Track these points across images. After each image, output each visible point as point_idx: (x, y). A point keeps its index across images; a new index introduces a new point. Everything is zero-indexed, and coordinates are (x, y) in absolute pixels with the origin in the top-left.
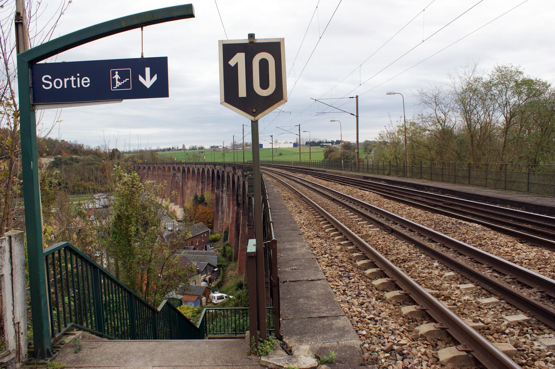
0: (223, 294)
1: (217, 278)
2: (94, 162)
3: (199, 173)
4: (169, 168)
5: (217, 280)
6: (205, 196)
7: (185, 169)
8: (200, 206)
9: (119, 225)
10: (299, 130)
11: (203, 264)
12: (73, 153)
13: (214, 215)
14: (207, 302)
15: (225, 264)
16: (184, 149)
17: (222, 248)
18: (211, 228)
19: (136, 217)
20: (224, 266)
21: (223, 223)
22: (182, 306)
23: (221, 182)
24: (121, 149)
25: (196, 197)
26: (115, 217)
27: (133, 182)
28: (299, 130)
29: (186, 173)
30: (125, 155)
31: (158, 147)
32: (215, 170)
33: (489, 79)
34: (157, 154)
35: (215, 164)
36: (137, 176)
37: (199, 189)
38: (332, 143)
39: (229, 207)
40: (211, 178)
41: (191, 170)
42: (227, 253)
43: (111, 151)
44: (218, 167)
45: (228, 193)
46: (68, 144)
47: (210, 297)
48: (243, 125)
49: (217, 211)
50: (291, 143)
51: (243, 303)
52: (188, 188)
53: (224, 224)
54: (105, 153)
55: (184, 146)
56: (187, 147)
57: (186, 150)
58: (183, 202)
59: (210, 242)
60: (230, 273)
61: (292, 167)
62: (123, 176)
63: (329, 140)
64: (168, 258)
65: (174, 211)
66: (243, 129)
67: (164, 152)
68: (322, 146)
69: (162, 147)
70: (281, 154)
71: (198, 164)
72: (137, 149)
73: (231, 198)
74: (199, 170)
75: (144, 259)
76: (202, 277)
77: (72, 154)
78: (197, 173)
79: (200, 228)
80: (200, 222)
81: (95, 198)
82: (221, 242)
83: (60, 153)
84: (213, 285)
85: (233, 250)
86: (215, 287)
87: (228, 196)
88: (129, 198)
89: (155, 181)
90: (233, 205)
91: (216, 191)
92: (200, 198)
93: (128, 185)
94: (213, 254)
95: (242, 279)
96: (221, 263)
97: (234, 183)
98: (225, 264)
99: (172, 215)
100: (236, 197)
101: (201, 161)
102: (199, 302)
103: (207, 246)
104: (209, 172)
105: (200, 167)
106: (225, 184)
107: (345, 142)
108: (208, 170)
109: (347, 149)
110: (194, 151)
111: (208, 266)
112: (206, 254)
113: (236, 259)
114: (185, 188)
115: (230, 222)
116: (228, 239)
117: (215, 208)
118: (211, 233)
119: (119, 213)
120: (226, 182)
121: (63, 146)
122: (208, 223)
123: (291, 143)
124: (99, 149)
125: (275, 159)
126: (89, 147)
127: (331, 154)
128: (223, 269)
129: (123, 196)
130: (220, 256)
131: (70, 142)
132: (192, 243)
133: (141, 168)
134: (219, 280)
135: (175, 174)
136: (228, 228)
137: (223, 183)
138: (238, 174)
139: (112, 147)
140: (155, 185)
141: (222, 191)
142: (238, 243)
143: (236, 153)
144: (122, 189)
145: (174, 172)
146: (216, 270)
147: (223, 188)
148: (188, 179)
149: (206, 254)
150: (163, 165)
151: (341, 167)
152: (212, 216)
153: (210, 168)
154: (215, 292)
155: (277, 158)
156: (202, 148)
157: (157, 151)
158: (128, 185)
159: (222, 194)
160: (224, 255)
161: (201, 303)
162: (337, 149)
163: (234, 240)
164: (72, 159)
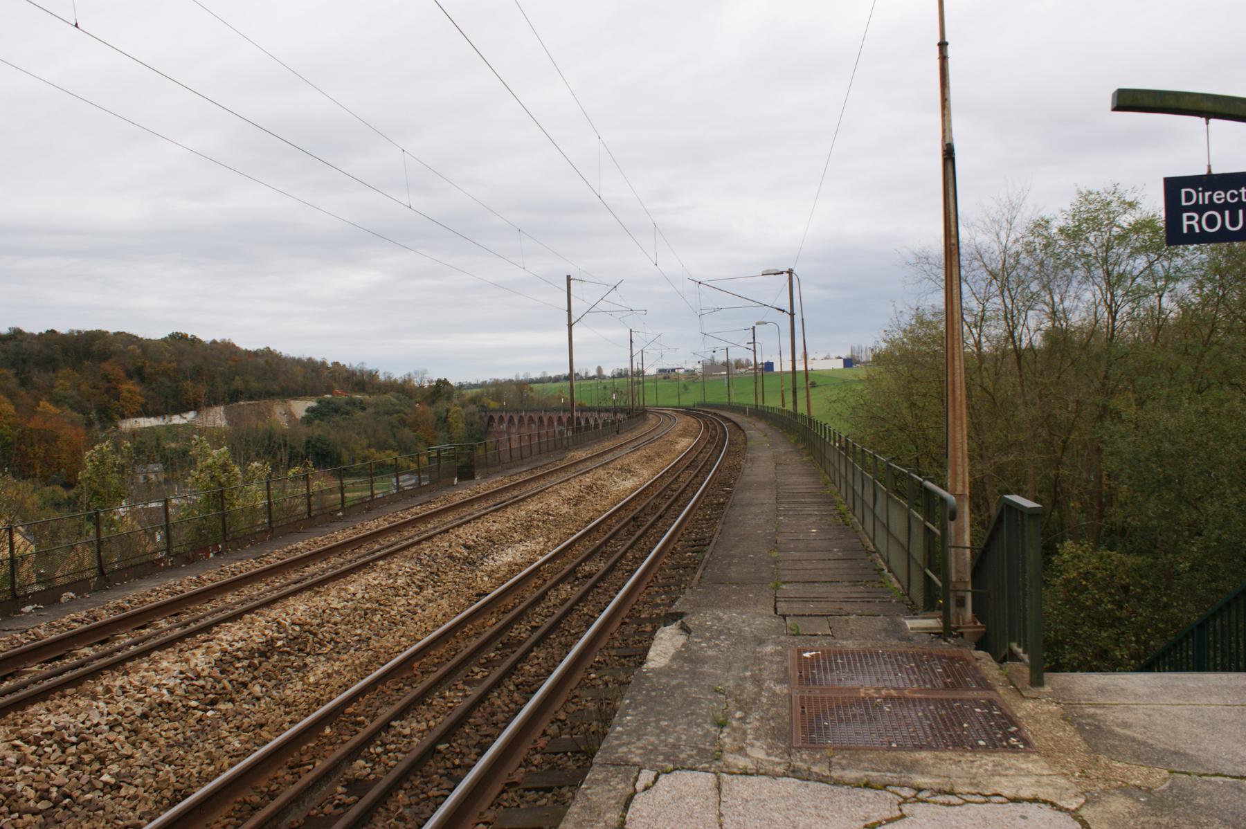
2: (397, 407)
4: (550, 419)
12: (357, 389)
16: (600, 376)
24: (453, 381)
30: (464, 392)
31: (544, 373)
34: (531, 389)
46: (347, 371)
50: (840, 358)
54: (421, 387)
55: (599, 370)
56: (607, 372)
57: (604, 378)
77: (355, 391)
83: (330, 390)
121: (337, 374)
123: (840, 358)
124: (410, 380)
126: (389, 377)
131: (351, 366)
139: (435, 375)
145: (560, 427)
164: (353, 403)
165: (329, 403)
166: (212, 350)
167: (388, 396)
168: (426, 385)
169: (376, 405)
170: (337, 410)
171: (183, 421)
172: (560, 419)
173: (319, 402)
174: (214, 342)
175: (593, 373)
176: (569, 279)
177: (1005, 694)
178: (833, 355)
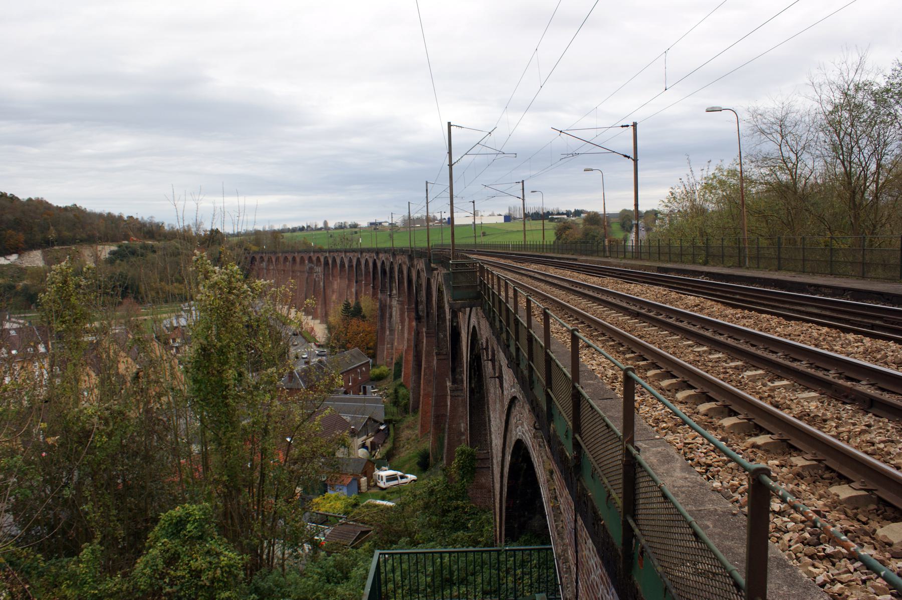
1: (384, 442)
3: (351, 266)
5: (385, 445)
6: (363, 305)
7: (328, 261)
8: (354, 321)
9: (205, 366)
10: (523, 189)
13: (377, 335)
14: (369, 485)
17: (391, 391)
18: (373, 356)
19: (238, 349)
20: (395, 421)
22: (327, 495)
23: (387, 280)
25: (347, 306)
26: (197, 350)
27: (230, 282)
28: (523, 189)
29: (331, 266)
30: (230, 239)
31: (285, 225)
32: (377, 261)
33: (883, 84)
34: (283, 236)
35: (378, 251)
36: (239, 272)
37: (351, 292)
38: (568, 214)
39: (402, 321)
40: (371, 274)
41: (338, 262)
43: (208, 233)
44: (382, 256)
45: (400, 299)
46: (139, 223)
49: (383, 329)
50: (500, 215)
52: (333, 292)
53: (394, 351)
55: (326, 223)
56: (331, 225)
58: (326, 315)
60: (406, 434)
61: (511, 254)
62: (212, 271)
63: (563, 209)
64: (299, 426)
65: (312, 329)
67: (295, 234)
68: (552, 220)
69: (290, 226)
70: (484, 234)
71: (349, 252)
72: (250, 228)
74: (350, 261)
75: (254, 431)
76: (359, 441)
78: (349, 266)
79: (354, 358)
81: (182, 309)
82: (389, 380)
83: (127, 237)
85: (411, 394)
86: (382, 459)
87: (401, 303)
88: (222, 315)
89: (273, 281)
90: (410, 319)
91: (379, 296)
92: (355, 308)
93: (220, 289)
94: (376, 401)
95: (428, 444)
96: (390, 417)
98: (399, 418)
99: (308, 337)
100: (414, 306)
101: (355, 246)
103: (367, 387)
104: (368, 264)
105: (354, 256)
106: (396, 285)
107: (589, 213)
108: (367, 261)
109: (592, 225)
110: (342, 230)
112: (364, 401)
113: (415, 410)
114: (329, 292)
115: (405, 347)
116: (401, 375)
117: (379, 324)
118: (373, 366)
119: (205, 342)
121: (131, 225)
122: (368, 348)
123: (500, 215)
125: (479, 240)
127: (567, 232)
128: (394, 425)
129: (211, 310)
130: (389, 405)
131: (142, 218)
134: (388, 446)
135: (311, 269)
136: (401, 358)
137: (391, 282)
138: (418, 267)
139: (207, 226)
140: (273, 289)
141: (390, 295)
142: (420, 383)
143: (412, 233)
144: (209, 296)
145: (311, 265)
146: (382, 427)
147: (391, 291)
148: (333, 276)
149: (364, 401)
150: (293, 255)
151: (604, 251)
152: (375, 338)
153: (370, 257)
155: (482, 240)
156: (355, 226)
157: (283, 231)
158: (220, 289)
159: (391, 301)
160: (396, 403)
161: (359, 487)
162: (576, 224)
163: (412, 378)
164: (145, 247)
165: (127, 247)
166: (29, 205)
167: (173, 242)
168: (202, 233)
169: (165, 248)
170: (134, 253)
171: (7, 262)
172: (310, 258)
173: (119, 247)
174: (30, 200)
175: (320, 225)
176: (449, 125)
177: (797, 485)
178: (496, 213)
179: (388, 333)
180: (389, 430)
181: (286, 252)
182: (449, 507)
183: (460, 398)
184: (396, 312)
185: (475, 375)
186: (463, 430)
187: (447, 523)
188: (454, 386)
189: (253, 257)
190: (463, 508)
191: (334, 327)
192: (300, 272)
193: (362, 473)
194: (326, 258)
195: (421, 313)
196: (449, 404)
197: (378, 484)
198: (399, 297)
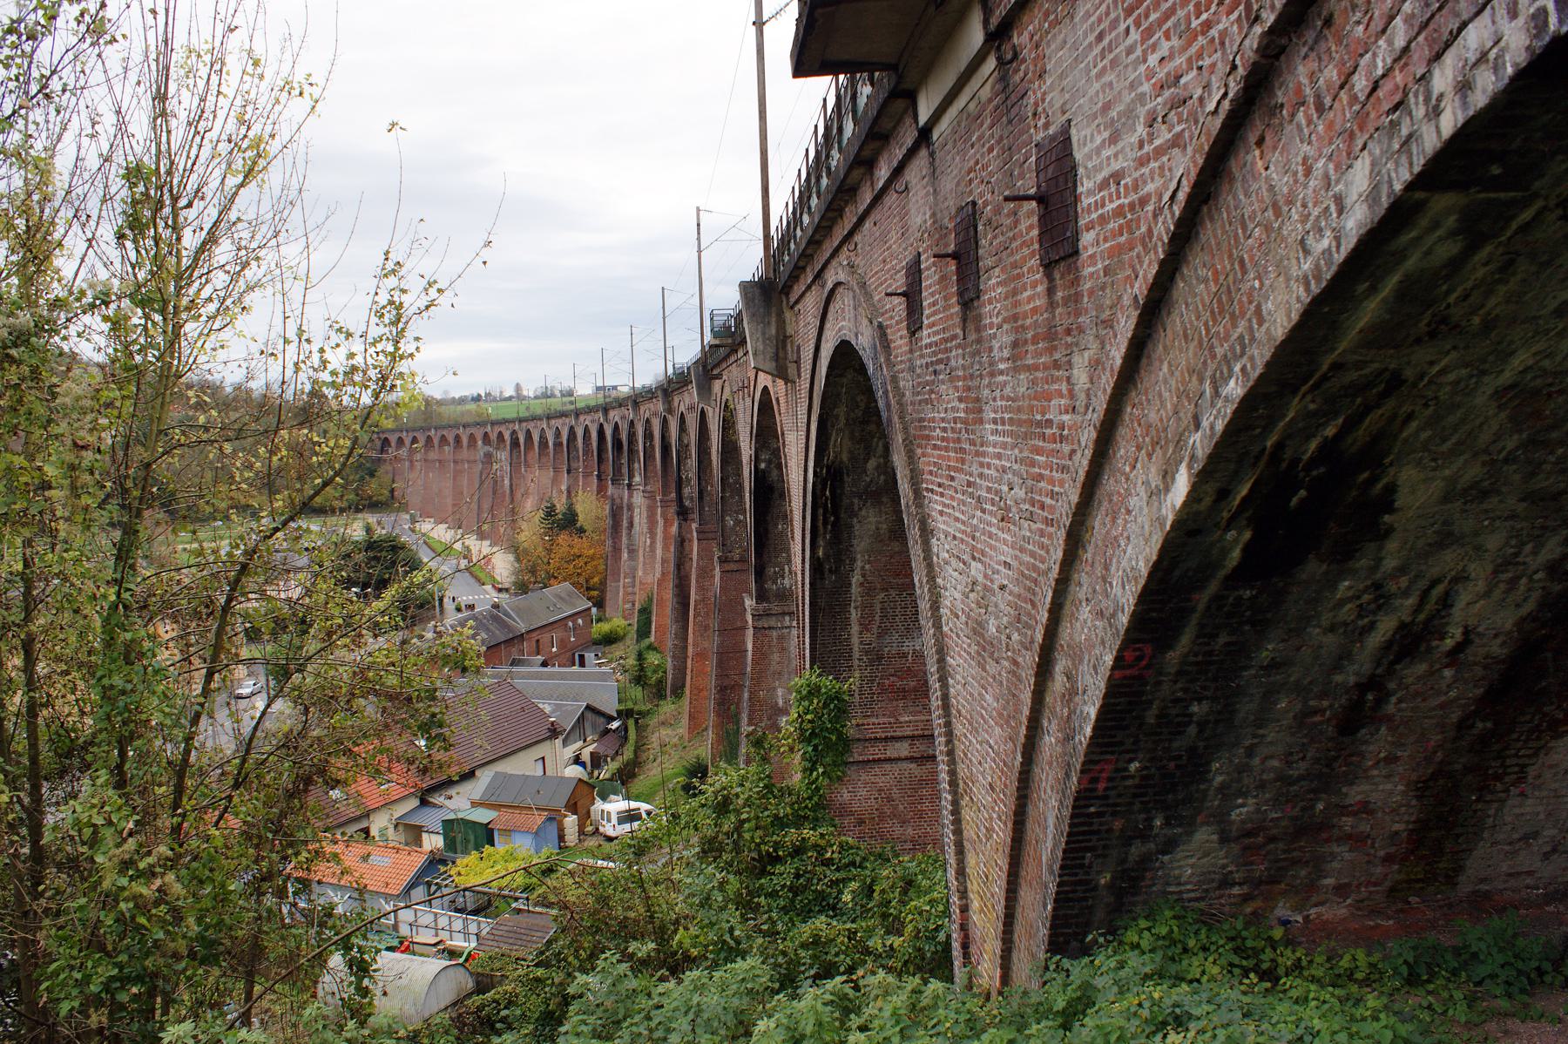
0: (634, 805)
3: (558, 445)
6: (579, 508)
8: (563, 538)
11: (570, 708)
14: (581, 832)
15: (643, 708)
16: (519, 396)
17: (631, 661)
20: (639, 713)
21: (634, 586)
23: (624, 461)
25: (550, 512)
31: (446, 392)
40: (595, 454)
41: (536, 438)
42: (649, 674)
45: (648, 488)
47: (592, 813)
48: (698, 210)
49: (617, 550)
51: (747, 836)
53: (637, 589)
55: (518, 387)
57: (525, 398)
59: (597, 643)
60: (659, 736)
66: (698, 225)
73: (658, 498)
74: (558, 434)
78: (555, 445)
80: (565, 580)
82: (628, 642)
84: (604, 774)
85: (669, 660)
87: (650, 496)
96: (630, 705)
97: (666, 448)
99: (477, 572)
102: (552, 831)
103: (586, 655)
105: (564, 424)
106: (638, 466)
108: (587, 430)
111: (589, 715)
113: (678, 691)
115: (658, 575)
117: (609, 543)
118: (599, 620)
120: (642, 454)
122: (588, 589)
132: (538, 647)
133: (393, 444)
134: (628, 753)
135: (488, 456)
136: (650, 600)
137: (631, 462)
142: (686, 639)
145: (487, 448)
146: (615, 725)
147: (631, 476)
149: (579, 676)
150: (455, 431)
153: (593, 421)
154: (612, 797)
159: (631, 496)
160: (640, 679)
161: (561, 838)
163: (672, 629)
175: (510, 392)
179: (625, 555)
180: (626, 730)
181: (444, 428)
182: (777, 846)
183: (774, 633)
184: (640, 519)
185: (825, 523)
186: (781, 703)
187: (773, 895)
188: (761, 607)
189: (386, 439)
190: (820, 850)
191: (526, 551)
192: (468, 462)
193: (567, 807)
194: (514, 432)
195: (687, 503)
196: (750, 646)
197: (601, 829)
198: (646, 485)
